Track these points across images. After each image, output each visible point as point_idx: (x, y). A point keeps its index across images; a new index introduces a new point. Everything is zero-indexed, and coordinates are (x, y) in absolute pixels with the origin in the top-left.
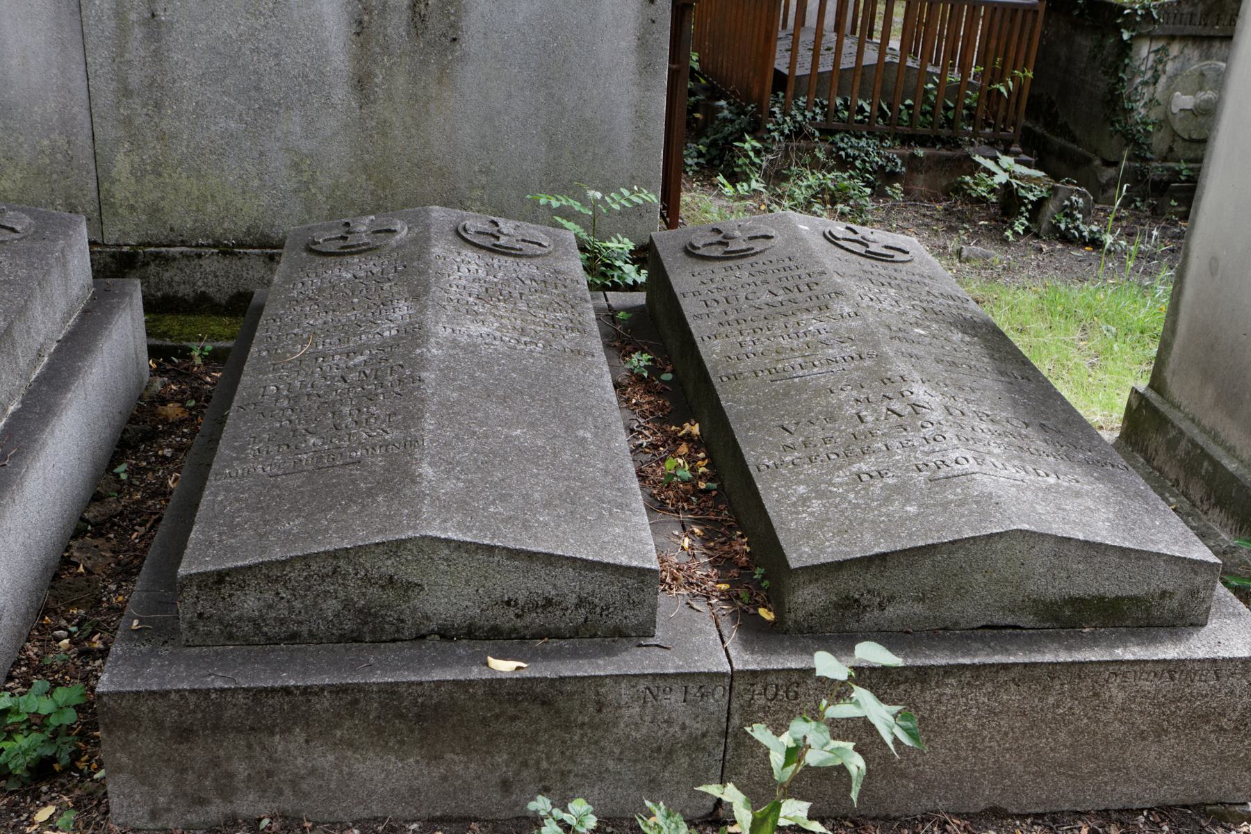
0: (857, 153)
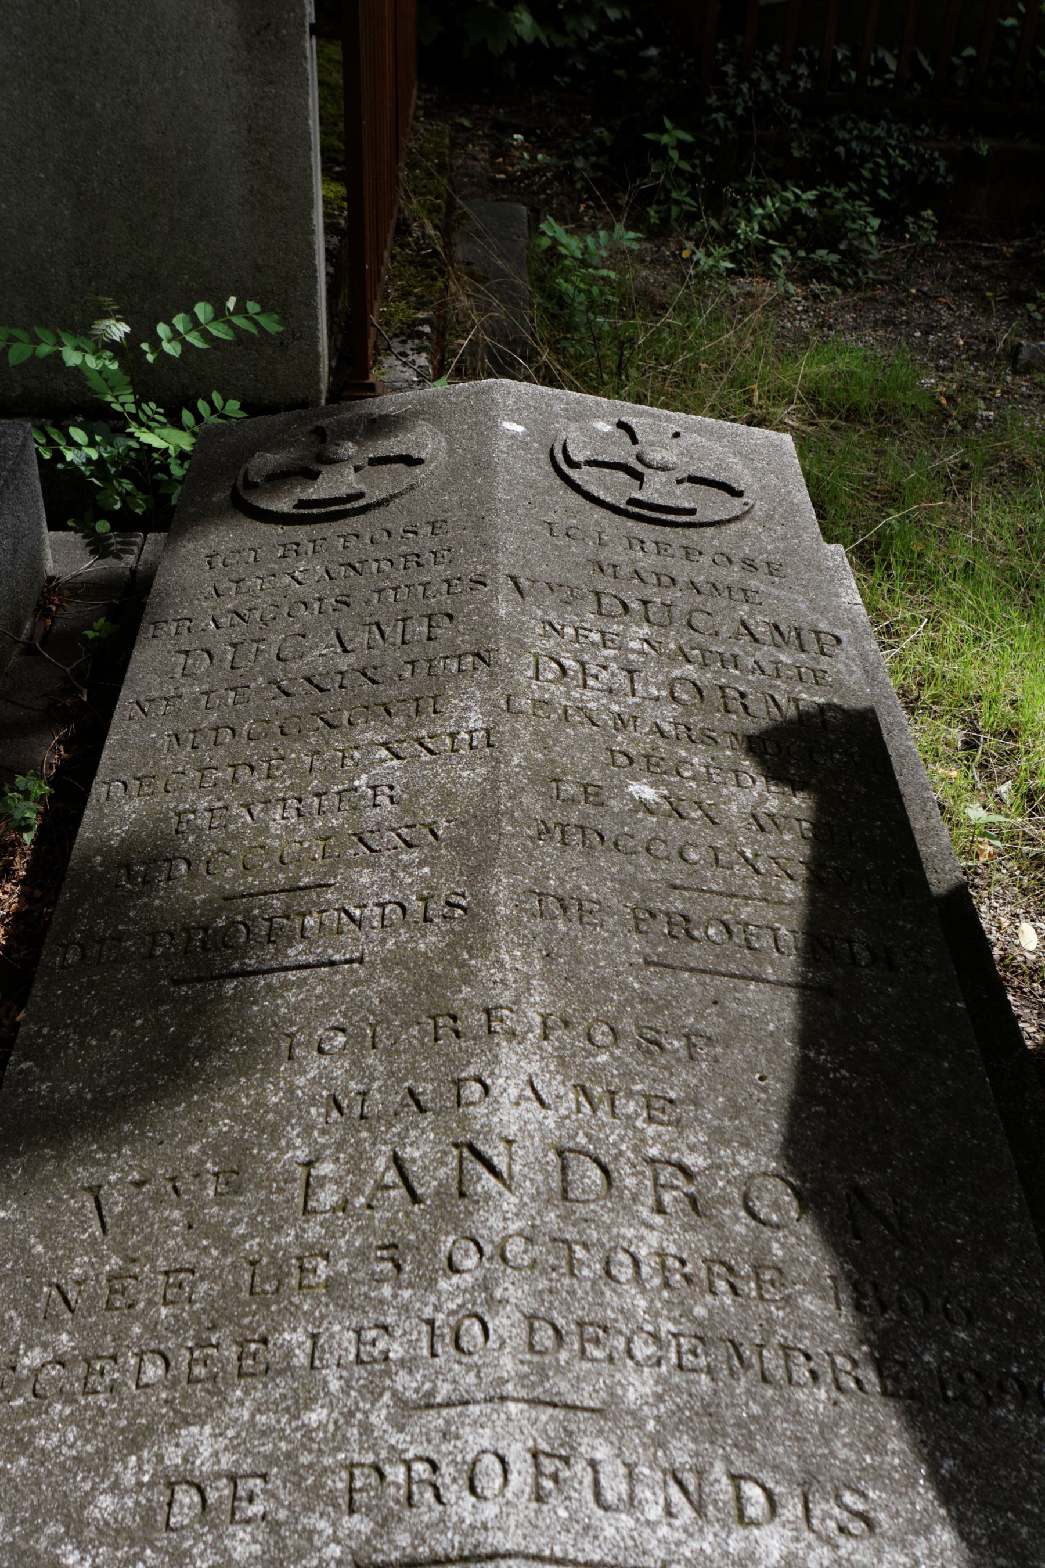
0: (867, 149)
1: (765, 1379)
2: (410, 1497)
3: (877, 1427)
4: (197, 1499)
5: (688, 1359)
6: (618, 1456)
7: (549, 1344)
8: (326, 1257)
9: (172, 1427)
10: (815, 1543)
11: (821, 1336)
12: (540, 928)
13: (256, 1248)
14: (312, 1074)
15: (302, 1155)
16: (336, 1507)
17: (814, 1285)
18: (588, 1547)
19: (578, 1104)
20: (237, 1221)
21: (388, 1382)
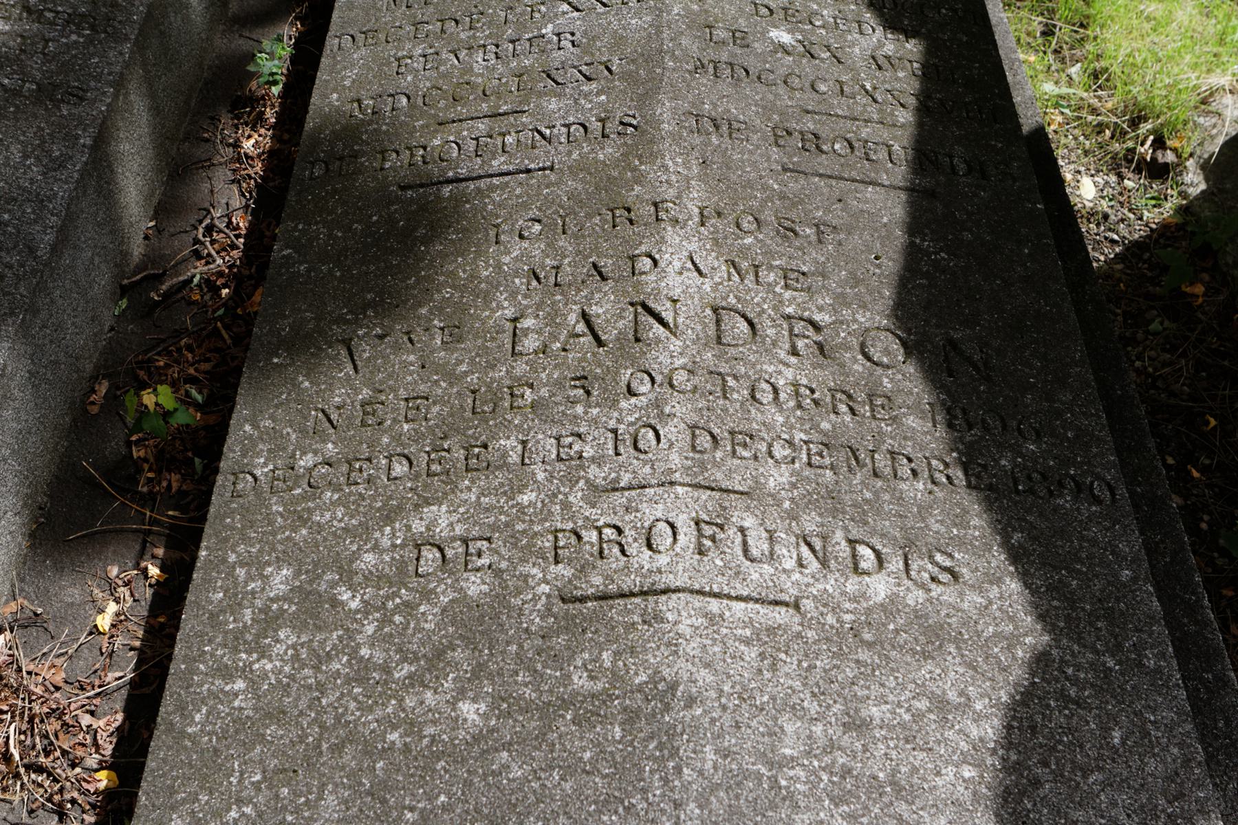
1: (876, 475)
2: (601, 552)
3: (963, 509)
4: (438, 555)
5: (816, 460)
6: (761, 525)
7: (707, 445)
8: (531, 386)
9: (417, 506)
10: (913, 588)
11: (921, 446)
12: (698, 141)
13: (475, 381)
14: (515, 254)
15: (509, 313)
16: (545, 559)
17: (915, 409)
18: (738, 585)
19: (729, 274)
20: (461, 362)
21: (582, 473)
